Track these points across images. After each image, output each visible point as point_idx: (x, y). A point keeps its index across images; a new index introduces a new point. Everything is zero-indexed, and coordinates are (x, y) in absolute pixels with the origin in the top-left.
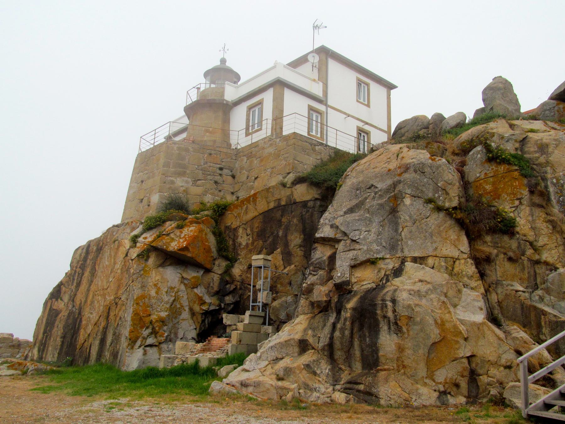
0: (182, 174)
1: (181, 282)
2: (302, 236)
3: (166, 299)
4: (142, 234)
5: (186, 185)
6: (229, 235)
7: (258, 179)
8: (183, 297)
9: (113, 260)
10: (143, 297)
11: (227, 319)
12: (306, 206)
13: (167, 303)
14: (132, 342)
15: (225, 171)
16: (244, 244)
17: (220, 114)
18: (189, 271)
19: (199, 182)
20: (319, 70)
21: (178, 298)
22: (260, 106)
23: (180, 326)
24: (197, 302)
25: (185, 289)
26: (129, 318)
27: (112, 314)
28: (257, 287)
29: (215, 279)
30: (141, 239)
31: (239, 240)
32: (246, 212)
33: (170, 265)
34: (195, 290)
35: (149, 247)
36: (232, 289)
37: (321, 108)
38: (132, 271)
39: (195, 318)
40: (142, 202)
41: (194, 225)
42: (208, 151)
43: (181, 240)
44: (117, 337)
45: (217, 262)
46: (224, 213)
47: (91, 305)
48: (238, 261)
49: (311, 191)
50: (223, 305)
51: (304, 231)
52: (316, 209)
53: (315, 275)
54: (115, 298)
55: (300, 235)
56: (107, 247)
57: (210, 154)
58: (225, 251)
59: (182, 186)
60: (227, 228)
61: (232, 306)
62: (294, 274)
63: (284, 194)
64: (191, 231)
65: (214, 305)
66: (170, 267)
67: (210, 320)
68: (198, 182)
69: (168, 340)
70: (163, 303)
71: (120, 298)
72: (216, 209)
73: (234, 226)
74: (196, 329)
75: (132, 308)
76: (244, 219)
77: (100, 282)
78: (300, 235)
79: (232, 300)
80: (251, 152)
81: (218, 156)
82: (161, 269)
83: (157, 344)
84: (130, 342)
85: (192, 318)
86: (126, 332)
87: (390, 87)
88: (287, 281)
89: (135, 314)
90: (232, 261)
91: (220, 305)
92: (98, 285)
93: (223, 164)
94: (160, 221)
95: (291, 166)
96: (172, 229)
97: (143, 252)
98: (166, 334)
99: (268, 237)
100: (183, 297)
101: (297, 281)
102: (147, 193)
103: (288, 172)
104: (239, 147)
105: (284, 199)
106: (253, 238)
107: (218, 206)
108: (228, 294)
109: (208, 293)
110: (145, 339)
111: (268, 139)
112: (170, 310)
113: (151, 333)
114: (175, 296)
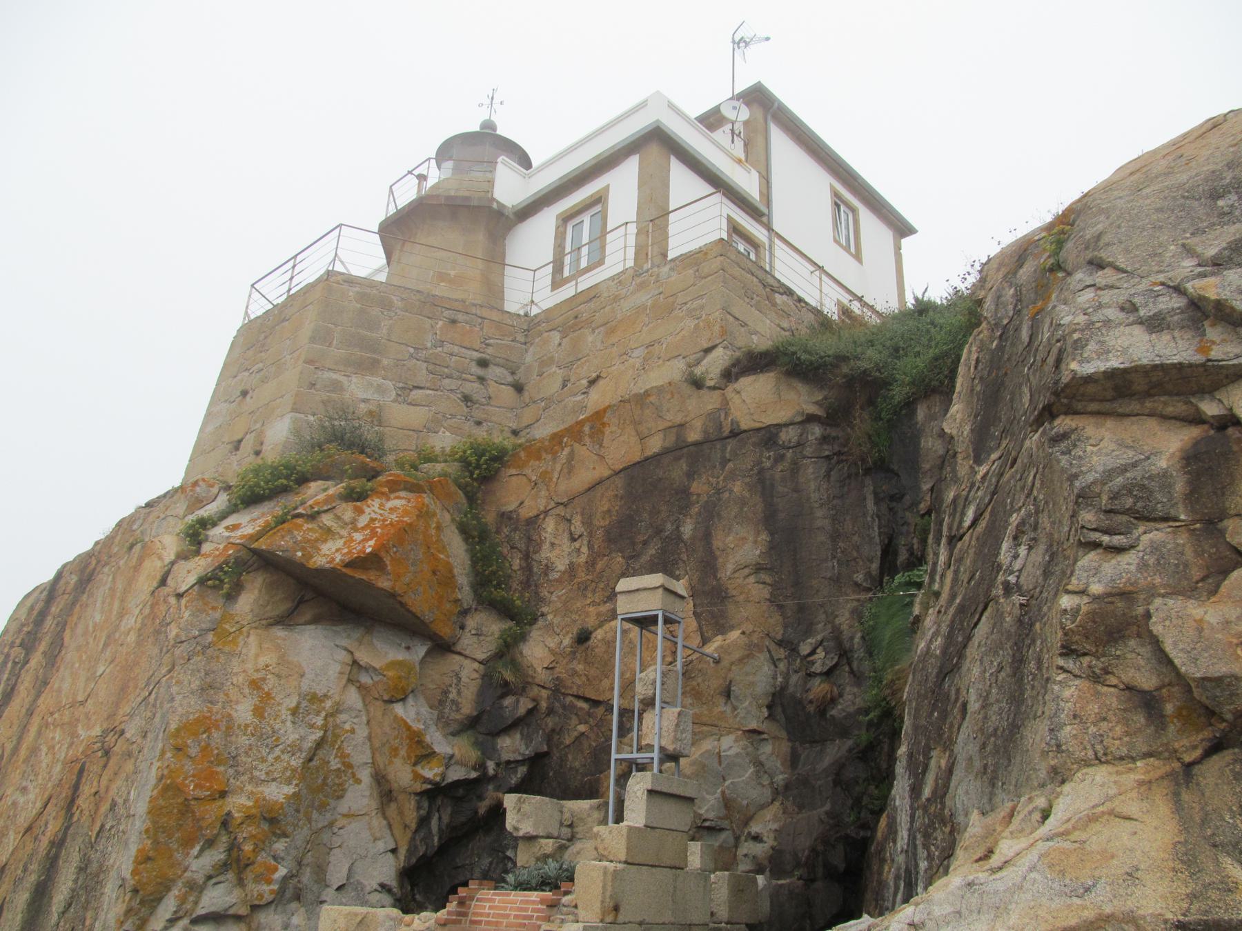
0: (368, 366)
1: (349, 680)
2: (764, 537)
3: (293, 737)
4: (224, 516)
5: (376, 397)
6: (509, 539)
7: (601, 383)
8: (353, 731)
9: (116, 604)
10: (204, 724)
11: (523, 814)
12: (775, 443)
13: (293, 749)
14: (142, 902)
15: (494, 372)
16: (561, 565)
17: (480, 237)
18: (378, 644)
19: (416, 394)
20: (746, 145)
21: (336, 736)
22: (598, 208)
23: (336, 841)
24: (403, 752)
25: (360, 705)
26: (141, 807)
27: (87, 790)
28: (641, 690)
29: (464, 675)
30: (218, 531)
31: (545, 553)
32: (570, 468)
33: (315, 621)
34: (399, 709)
35: (243, 554)
36: (522, 711)
37: (758, 232)
38: (173, 631)
39: (392, 809)
40: (237, 448)
41: (402, 494)
42: (446, 313)
43: (358, 536)
44: (90, 877)
45: (471, 623)
46: (498, 471)
47: (27, 760)
48: (540, 623)
49: (791, 396)
50: (491, 765)
51: (769, 520)
52: (808, 451)
53: (1119, 550)
54: (105, 733)
55: (758, 533)
56: (106, 569)
57: (454, 322)
58: (498, 586)
59: (364, 401)
60: (505, 517)
61: (522, 770)
62: (741, 660)
63: (695, 412)
64: (392, 510)
65: (461, 763)
66: (312, 627)
67: (446, 819)
68: (415, 392)
69: (288, 894)
70: (277, 752)
71: (122, 732)
72: (473, 459)
73: (526, 513)
74: (394, 851)
75: (157, 764)
76: (562, 487)
77: (67, 682)
78: (758, 533)
79: (523, 749)
80: (572, 319)
81: (477, 329)
82: (279, 632)
83: (243, 911)
84: (135, 903)
85: (382, 810)
86: (122, 861)
87: (902, 229)
88: (716, 684)
89: (166, 788)
90: (520, 618)
91: (481, 766)
92: (59, 690)
93: (490, 350)
94: (287, 477)
95: (717, 328)
96: (328, 500)
97: (220, 568)
98: (282, 871)
99: (645, 543)
100: (353, 731)
101: (752, 684)
102: (256, 422)
103: (706, 346)
104: (535, 311)
105: (698, 424)
106: (590, 547)
107: (479, 451)
108: (507, 730)
109: (442, 721)
110: (195, 888)
111: (631, 272)
112: (303, 778)
113: (224, 867)
114: (325, 728)
